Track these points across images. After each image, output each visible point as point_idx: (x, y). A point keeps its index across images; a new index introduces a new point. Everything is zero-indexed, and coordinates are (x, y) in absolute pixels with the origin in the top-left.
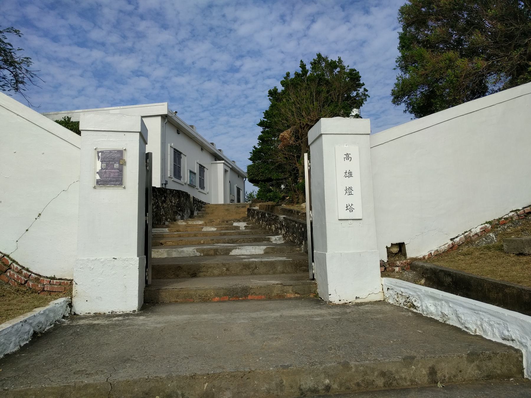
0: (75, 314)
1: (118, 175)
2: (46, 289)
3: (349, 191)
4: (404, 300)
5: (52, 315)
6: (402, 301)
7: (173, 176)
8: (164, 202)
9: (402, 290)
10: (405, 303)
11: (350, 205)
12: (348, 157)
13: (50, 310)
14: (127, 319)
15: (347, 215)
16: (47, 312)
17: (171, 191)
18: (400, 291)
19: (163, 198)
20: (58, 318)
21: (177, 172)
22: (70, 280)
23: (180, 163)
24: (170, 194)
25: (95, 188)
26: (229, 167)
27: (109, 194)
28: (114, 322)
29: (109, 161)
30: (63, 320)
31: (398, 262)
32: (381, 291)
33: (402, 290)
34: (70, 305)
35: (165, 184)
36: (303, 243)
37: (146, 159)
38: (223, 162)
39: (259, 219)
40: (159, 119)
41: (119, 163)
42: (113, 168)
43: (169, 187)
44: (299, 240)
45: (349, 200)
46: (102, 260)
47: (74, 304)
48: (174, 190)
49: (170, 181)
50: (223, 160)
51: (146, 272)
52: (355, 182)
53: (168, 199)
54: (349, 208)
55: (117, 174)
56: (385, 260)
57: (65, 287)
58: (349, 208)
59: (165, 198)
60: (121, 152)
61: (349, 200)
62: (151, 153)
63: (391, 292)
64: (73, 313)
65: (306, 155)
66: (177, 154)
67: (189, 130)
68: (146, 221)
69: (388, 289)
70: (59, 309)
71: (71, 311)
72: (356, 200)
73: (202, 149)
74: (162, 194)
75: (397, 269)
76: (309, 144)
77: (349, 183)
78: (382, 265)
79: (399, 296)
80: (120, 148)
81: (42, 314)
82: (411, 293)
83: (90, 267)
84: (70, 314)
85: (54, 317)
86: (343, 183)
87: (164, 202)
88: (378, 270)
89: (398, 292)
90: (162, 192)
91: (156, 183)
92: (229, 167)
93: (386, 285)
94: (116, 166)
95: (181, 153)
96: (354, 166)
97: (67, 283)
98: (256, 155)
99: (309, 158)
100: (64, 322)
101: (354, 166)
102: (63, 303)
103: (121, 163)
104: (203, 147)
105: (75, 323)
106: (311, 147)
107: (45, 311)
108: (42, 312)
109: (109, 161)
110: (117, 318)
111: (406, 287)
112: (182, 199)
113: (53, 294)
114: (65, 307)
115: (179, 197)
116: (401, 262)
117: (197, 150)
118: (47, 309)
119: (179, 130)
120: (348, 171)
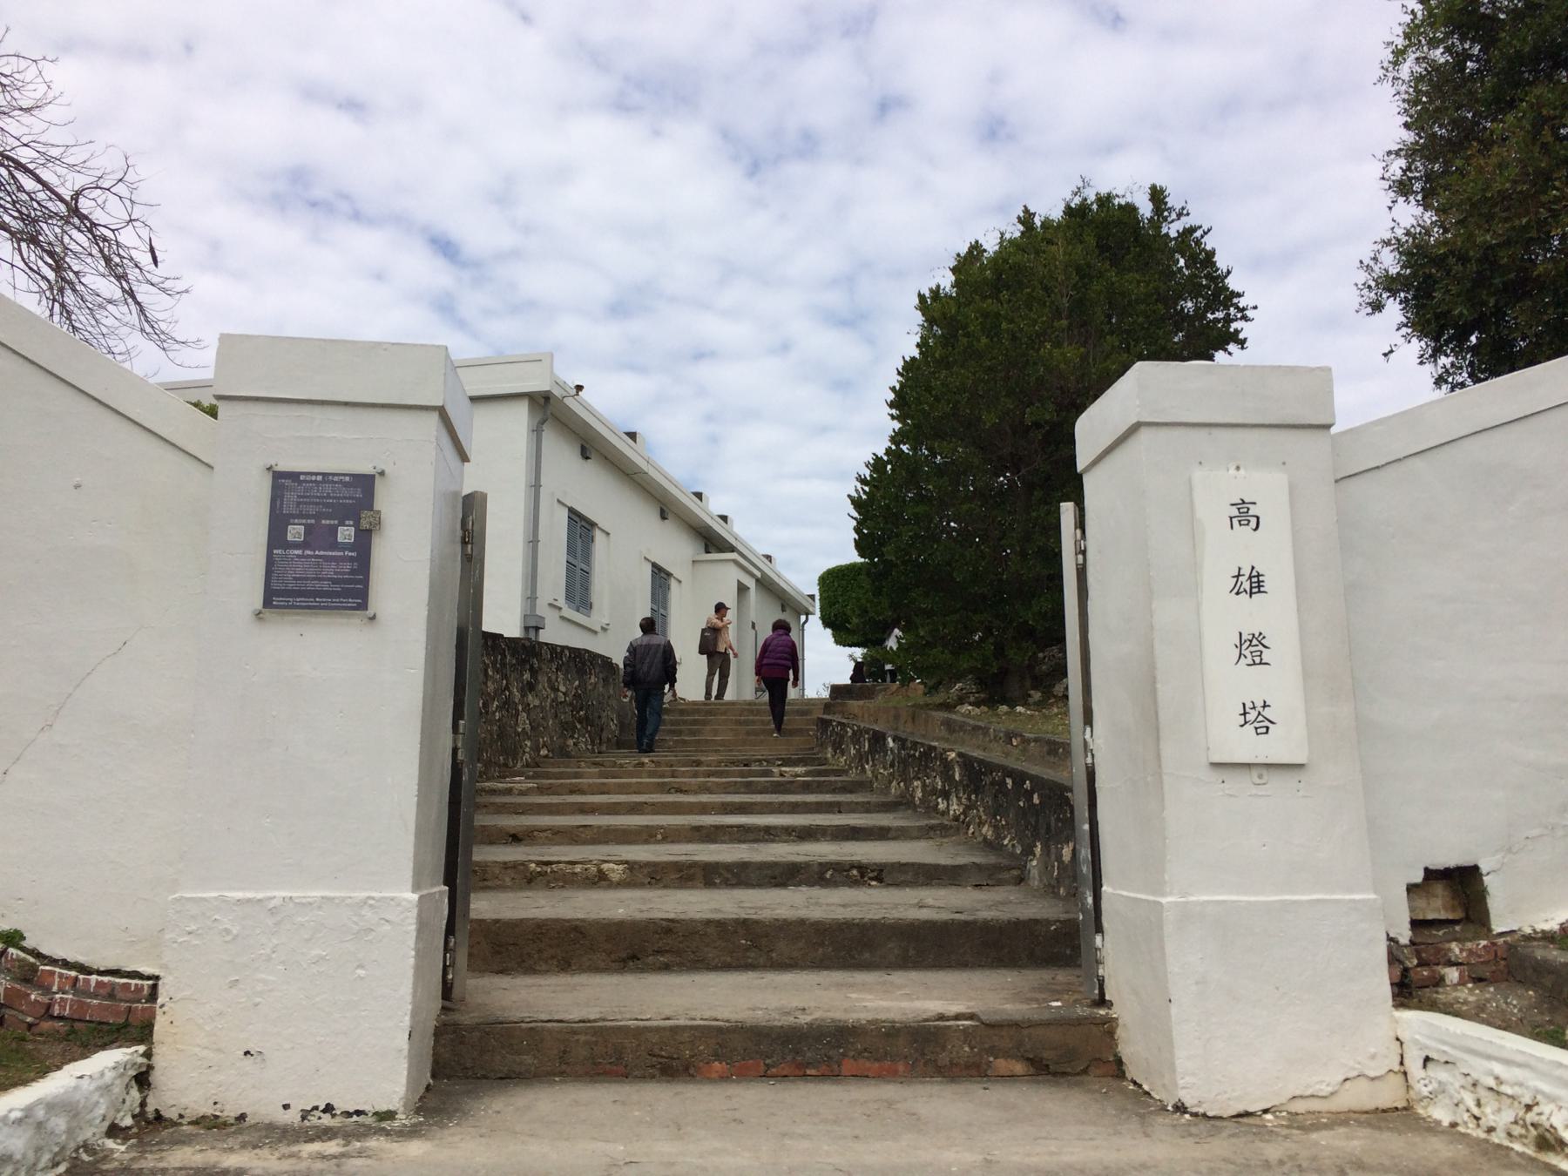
0: (159, 1117)
1: (353, 572)
2: (56, 1011)
3: (1252, 647)
4: (1507, 1116)
5: (60, 1123)
6: (1500, 1117)
7: (562, 602)
8: (531, 687)
9: (1498, 1069)
10: (1517, 1130)
11: (1259, 704)
12: (1244, 514)
13: (52, 1106)
14: (360, 1154)
15: (1246, 746)
16: (40, 1113)
17: (556, 651)
18: (1490, 1073)
19: (527, 676)
20: (87, 1134)
21: (579, 590)
22: (149, 978)
23: (587, 556)
24: (551, 660)
25: (258, 614)
26: (752, 575)
27: (318, 645)
28: (303, 1166)
29: (318, 516)
30: (110, 1144)
31: (1455, 947)
32: (1397, 1068)
33: (1498, 1069)
34: (143, 1079)
35: (537, 629)
36: (1038, 850)
37: (468, 525)
38: (734, 556)
39: (861, 758)
40: (521, 411)
41: (357, 525)
42: (335, 545)
43: (545, 636)
44: (1020, 837)
45: (1251, 684)
46: (272, 904)
47: (156, 1077)
48: (563, 648)
49: (551, 618)
50: (732, 549)
51: (446, 949)
52: (1274, 615)
53: (543, 679)
54: (1257, 718)
55: (347, 567)
56: (1404, 935)
57: (120, 1012)
58: (1257, 718)
59: (534, 672)
60: (365, 484)
61: (1251, 684)
62: (484, 497)
63: (1439, 1074)
64: (151, 1116)
65: (1067, 509)
66: (581, 528)
67: (624, 446)
68: (455, 751)
69: (1427, 1060)
70: (95, 1097)
71: (143, 1104)
72: (1280, 684)
73: (663, 517)
74: (524, 662)
75: (1453, 974)
76: (1080, 468)
77: (1251, 614)
78: (1393, 959)
79: (1482, 1093)
80: (366, 468)
81: (19, 1122)
82: (1545, 1087)
83: (227, 931)
84: (139, 1117)
85: (70, 1132)
86: (1228, 617)
87: (531, 687)
88: (1381, 983)
89: (1475, 1075)
90: (525, 654)
91: (502, 616)
92: (752, 575)
93: (1416, 1042)
94: (346, 534)
95: (593, 525)
96: (1269, 550)
97: (139, 989)
98: (884, 502)
99: (1081, 524)
100: (107, 1156)
101: (1269, 550)
102: (109, 1076)
103: (364, 525)
104: (666, 507)
105: (149, 1162)
106: (1086, 480)
107: (29, 1111)
108: (18, 1114)
109: (318, 516)
110: (316, 1147)
111: (1519, 1058)
112: (593, 680)
113: (86, 1036)
114: (118, 1089)
115: (582, 672)
116: (1469, 945)
117: (649, 516)
118: (39, 1102)
119: (590, 445)
120: (1246, 571)
